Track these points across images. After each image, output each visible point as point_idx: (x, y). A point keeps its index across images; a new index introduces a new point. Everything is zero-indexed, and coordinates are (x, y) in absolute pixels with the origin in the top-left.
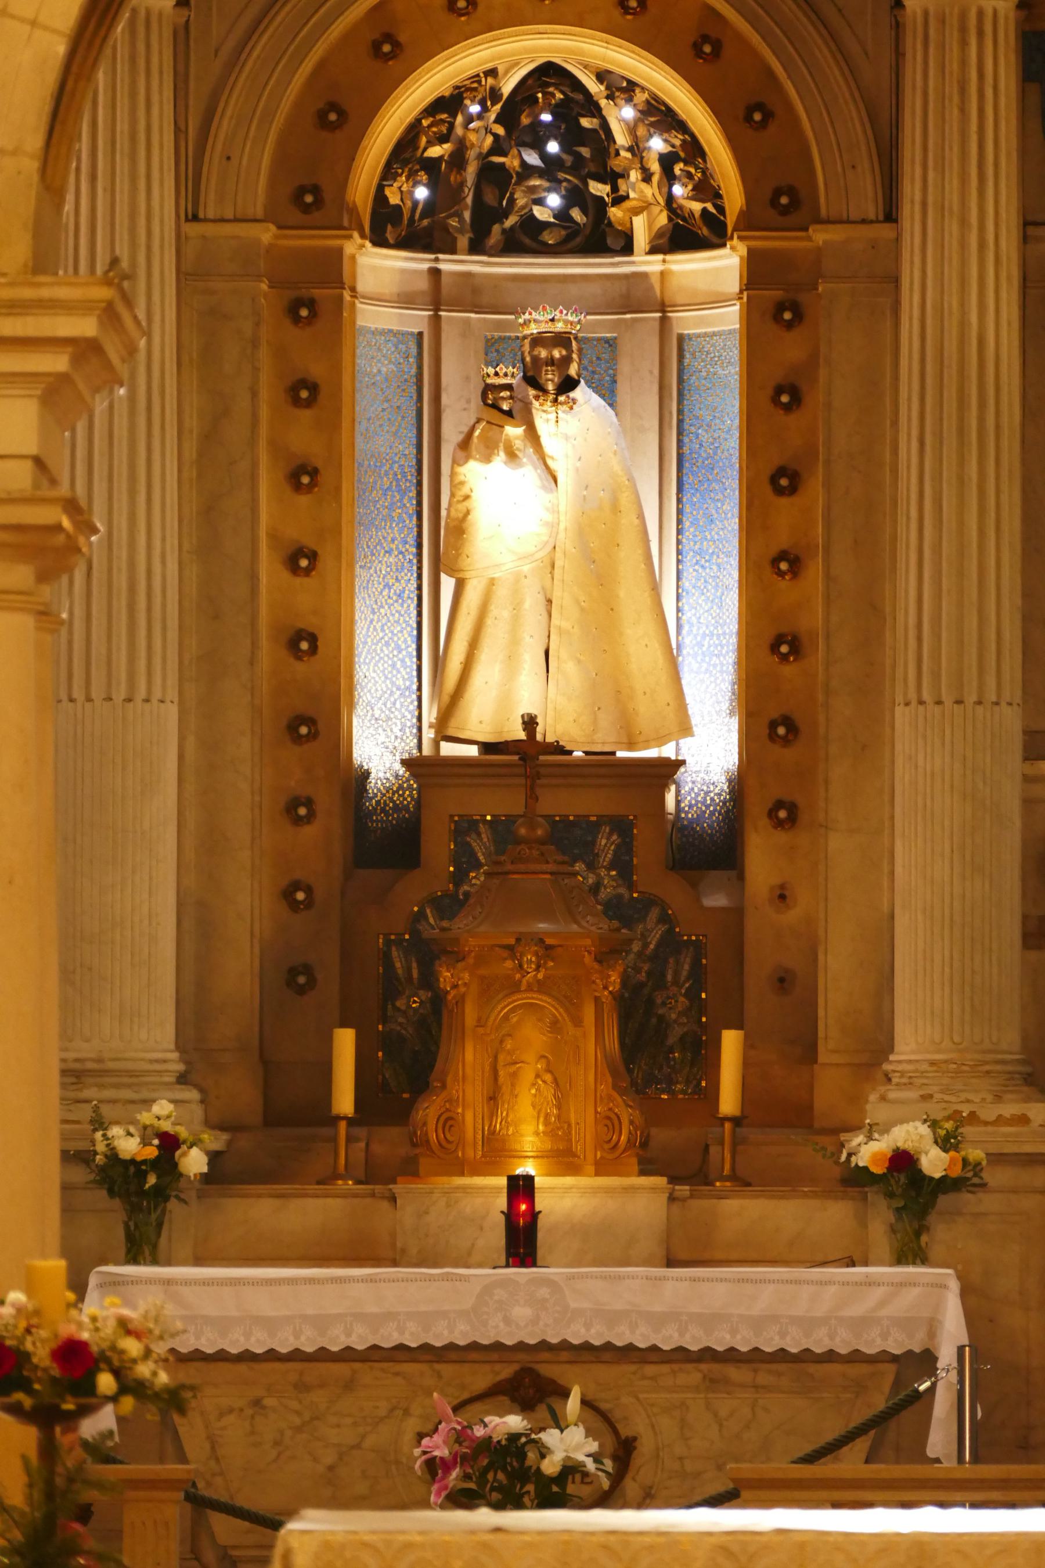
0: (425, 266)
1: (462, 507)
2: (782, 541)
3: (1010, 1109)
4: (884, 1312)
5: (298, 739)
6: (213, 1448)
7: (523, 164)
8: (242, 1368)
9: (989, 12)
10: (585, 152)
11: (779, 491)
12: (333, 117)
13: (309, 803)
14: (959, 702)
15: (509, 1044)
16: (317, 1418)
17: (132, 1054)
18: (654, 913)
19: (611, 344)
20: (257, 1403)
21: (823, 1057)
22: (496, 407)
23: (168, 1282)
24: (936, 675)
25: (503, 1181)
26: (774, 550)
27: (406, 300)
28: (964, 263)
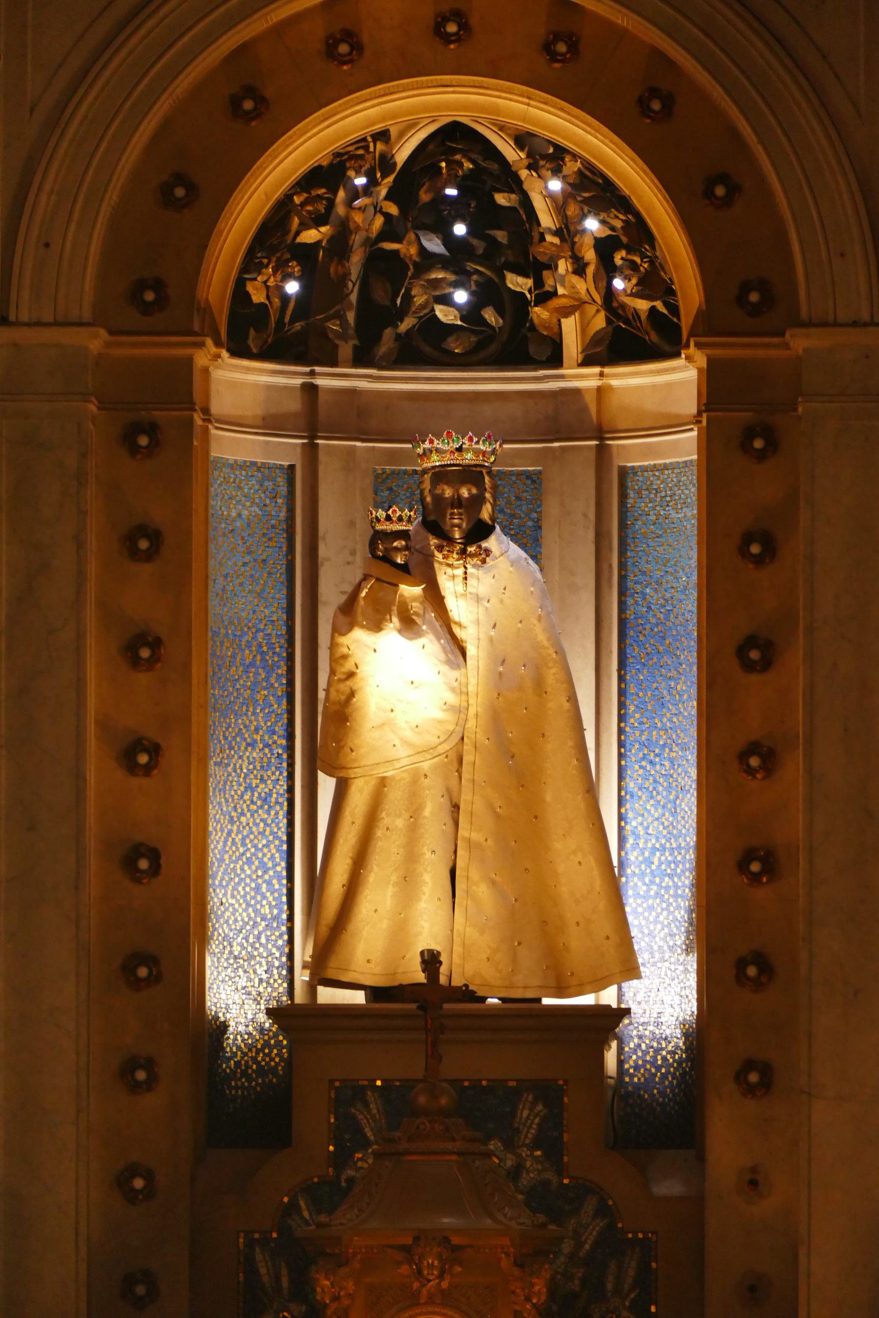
0: (298, 381)
5: (137, 984)
10: (501, 236)
11: (749, 666)
13: (149, 1065)
18: (590, 1205)
22: (387, 559)
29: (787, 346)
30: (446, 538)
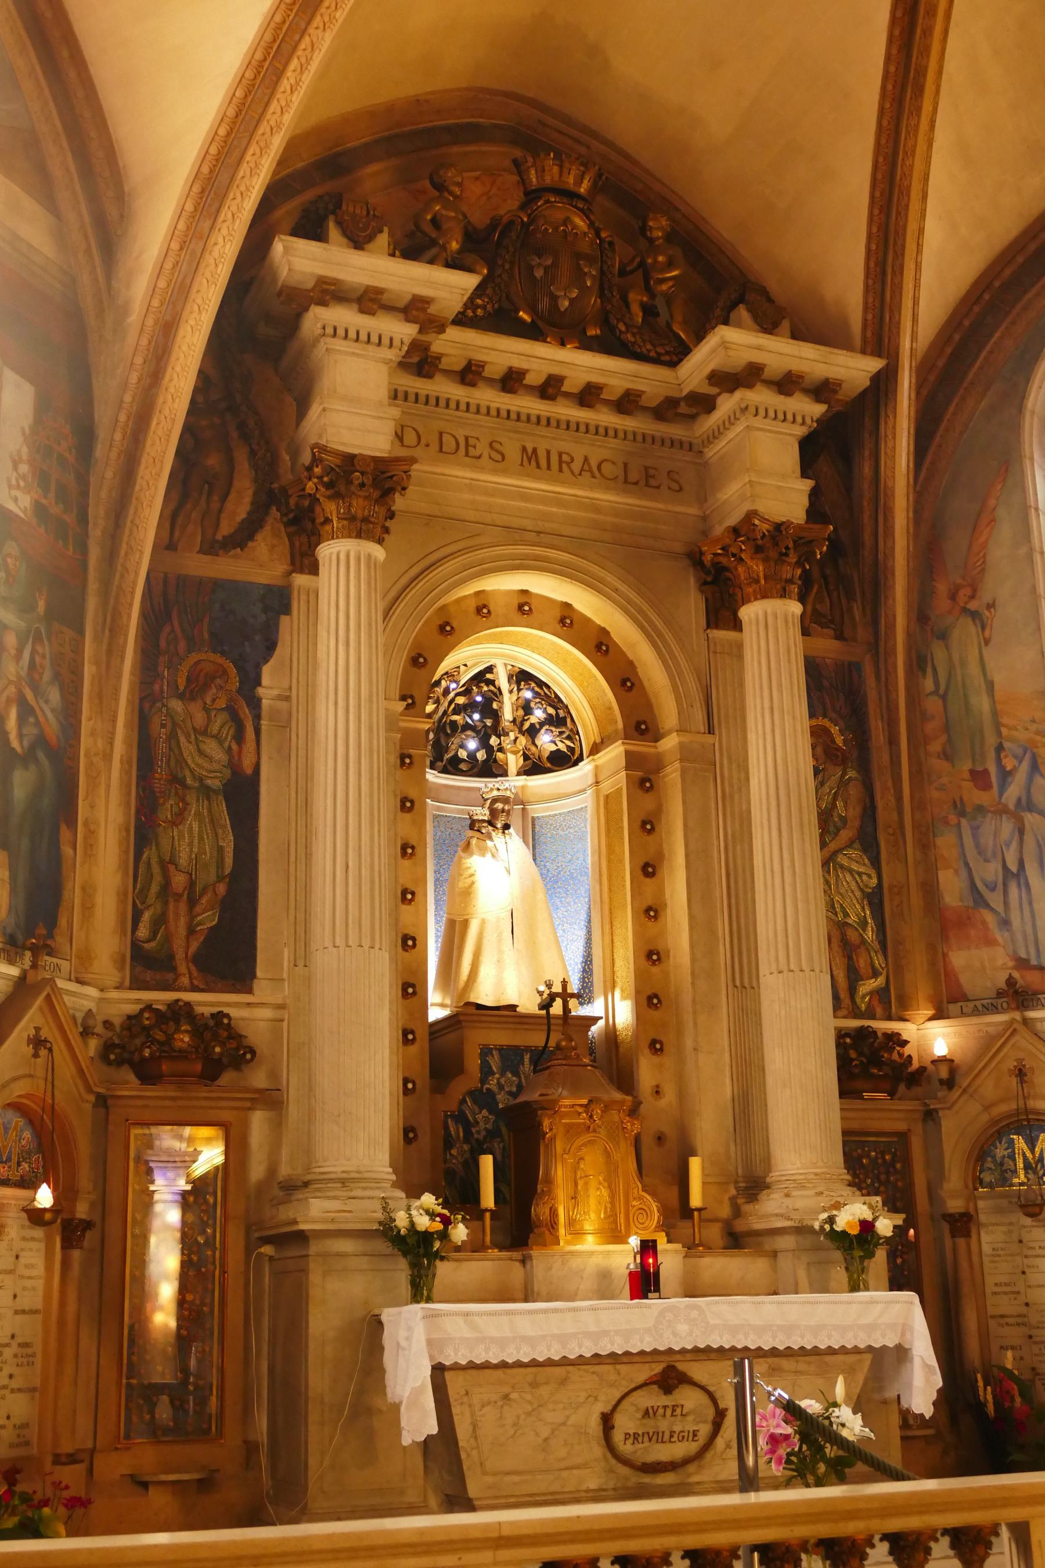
1: (469, 881)
6: (474, 1430)
8: (499, 1373)
16: (541, 1406)
17: (375, 1169)
20: (506, 1397)
23: (467, 1314)
26: (644, 906)
29: (656, 747)
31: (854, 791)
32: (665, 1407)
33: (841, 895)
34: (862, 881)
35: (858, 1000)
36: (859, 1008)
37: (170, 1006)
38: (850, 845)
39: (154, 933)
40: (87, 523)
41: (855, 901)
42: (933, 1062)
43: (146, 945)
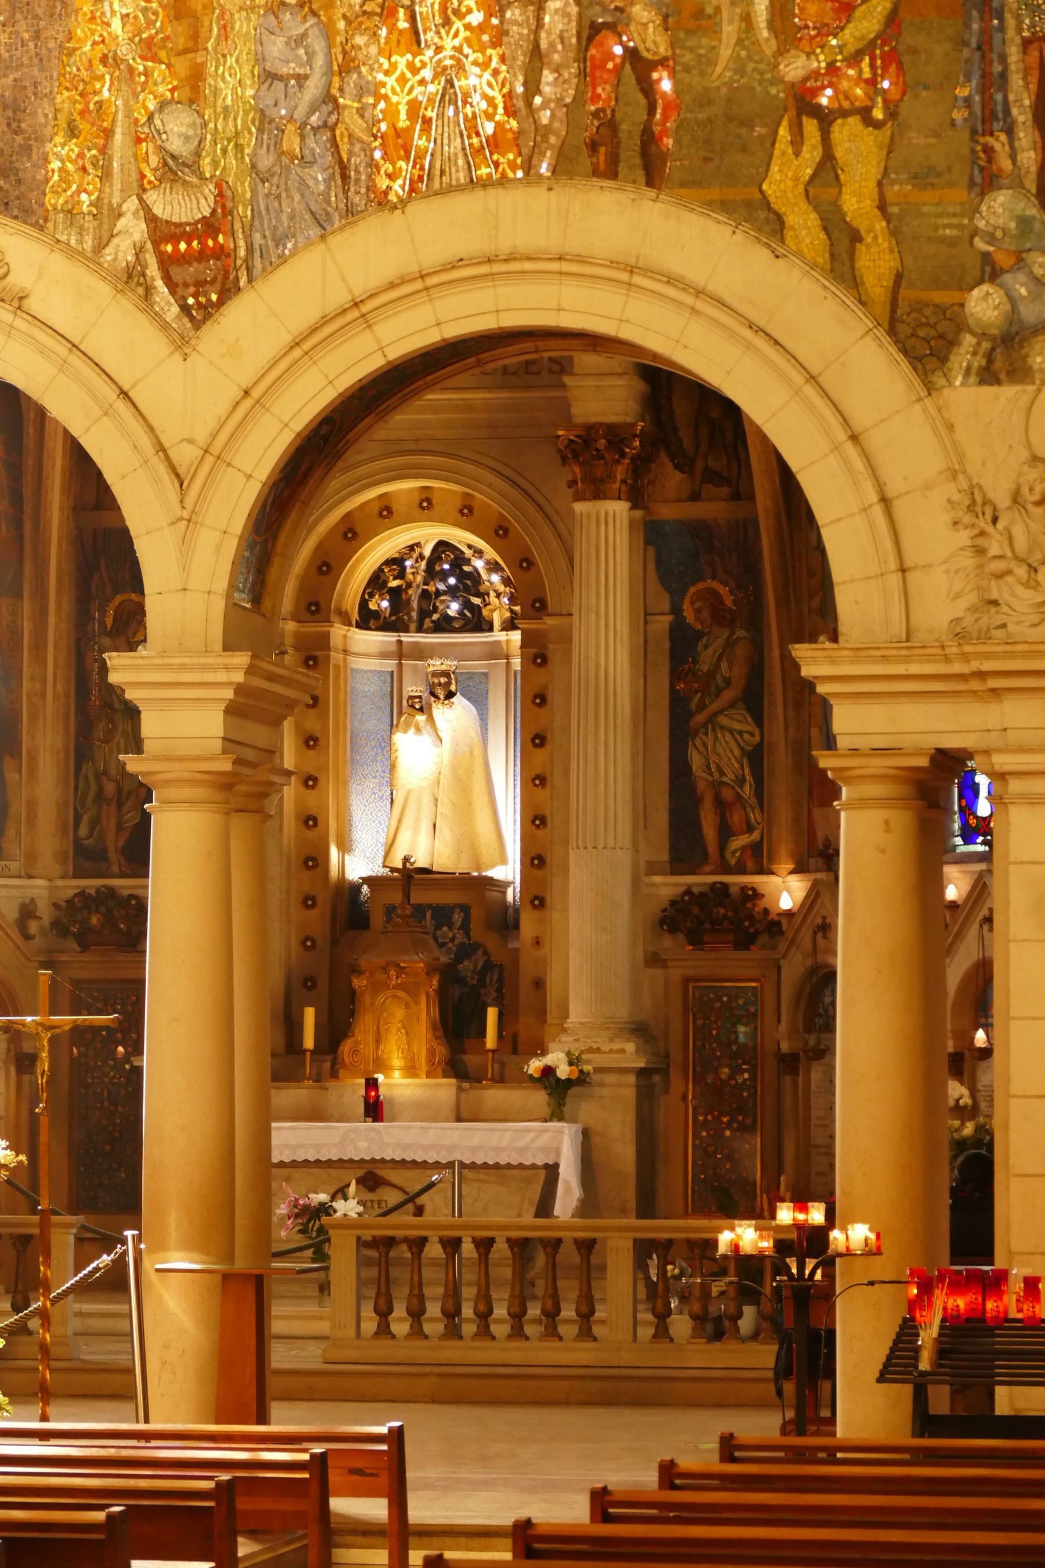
0: (395, 639)
2: (538, 770)
3: (615, 1046)
4: (534, 1145)
5: (308, 868)
7: (437, 590)
9: (611, 513)
10: (469, 582)
11: (536, 746)
12: (324, 569)
13: (313, 899)
14: (595, 848)
15: (385, 1015)
18: (480, 952)
19: (486, 675)
21: (549, 1020)
22: (412, 706)
24: (585, 835)
25: (363, 1081)
26: (533, 775)
27: (384, 655)
28: (597, 633)
30: (437, 697)
31: (741, 651)
32: (372, 1201)
33: (719, 755)
34: (743, 739)
35: (728, 855)
36: (728, 863)
37: (98, 890)
38: (733, 705)
39: (92, 831)
40: (22, 499)
41: (733, 760)
42: (778, 914)
43: (85, 842)
